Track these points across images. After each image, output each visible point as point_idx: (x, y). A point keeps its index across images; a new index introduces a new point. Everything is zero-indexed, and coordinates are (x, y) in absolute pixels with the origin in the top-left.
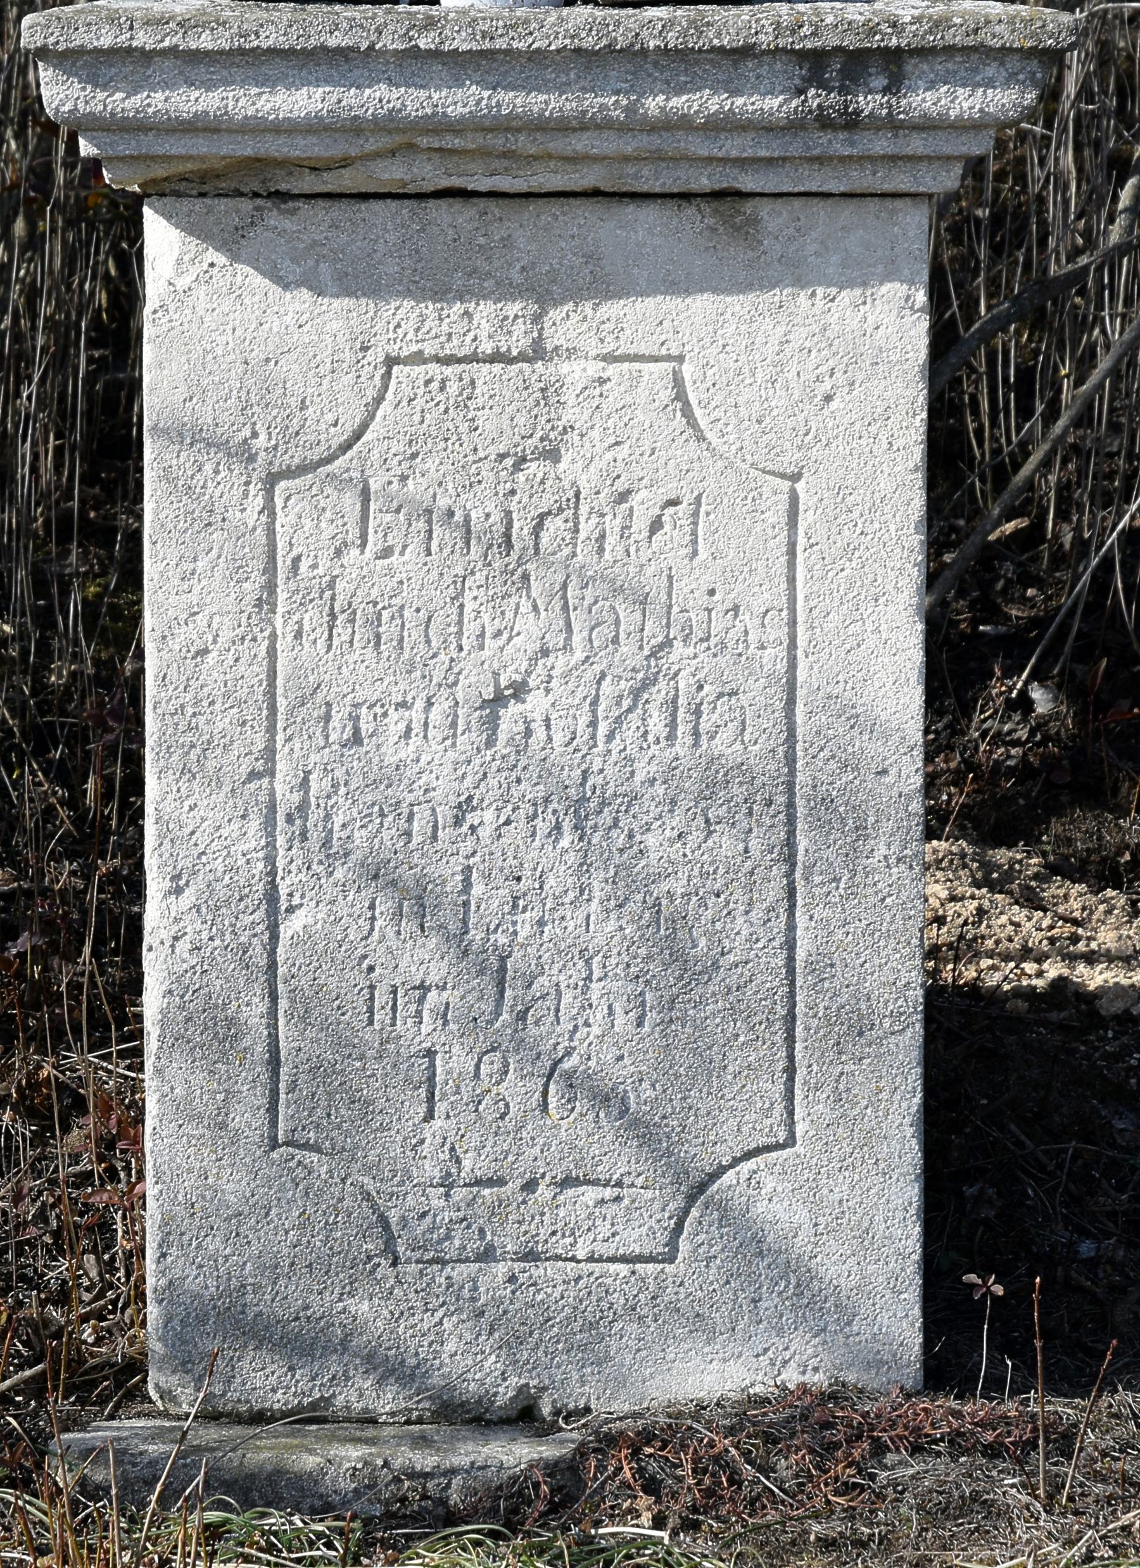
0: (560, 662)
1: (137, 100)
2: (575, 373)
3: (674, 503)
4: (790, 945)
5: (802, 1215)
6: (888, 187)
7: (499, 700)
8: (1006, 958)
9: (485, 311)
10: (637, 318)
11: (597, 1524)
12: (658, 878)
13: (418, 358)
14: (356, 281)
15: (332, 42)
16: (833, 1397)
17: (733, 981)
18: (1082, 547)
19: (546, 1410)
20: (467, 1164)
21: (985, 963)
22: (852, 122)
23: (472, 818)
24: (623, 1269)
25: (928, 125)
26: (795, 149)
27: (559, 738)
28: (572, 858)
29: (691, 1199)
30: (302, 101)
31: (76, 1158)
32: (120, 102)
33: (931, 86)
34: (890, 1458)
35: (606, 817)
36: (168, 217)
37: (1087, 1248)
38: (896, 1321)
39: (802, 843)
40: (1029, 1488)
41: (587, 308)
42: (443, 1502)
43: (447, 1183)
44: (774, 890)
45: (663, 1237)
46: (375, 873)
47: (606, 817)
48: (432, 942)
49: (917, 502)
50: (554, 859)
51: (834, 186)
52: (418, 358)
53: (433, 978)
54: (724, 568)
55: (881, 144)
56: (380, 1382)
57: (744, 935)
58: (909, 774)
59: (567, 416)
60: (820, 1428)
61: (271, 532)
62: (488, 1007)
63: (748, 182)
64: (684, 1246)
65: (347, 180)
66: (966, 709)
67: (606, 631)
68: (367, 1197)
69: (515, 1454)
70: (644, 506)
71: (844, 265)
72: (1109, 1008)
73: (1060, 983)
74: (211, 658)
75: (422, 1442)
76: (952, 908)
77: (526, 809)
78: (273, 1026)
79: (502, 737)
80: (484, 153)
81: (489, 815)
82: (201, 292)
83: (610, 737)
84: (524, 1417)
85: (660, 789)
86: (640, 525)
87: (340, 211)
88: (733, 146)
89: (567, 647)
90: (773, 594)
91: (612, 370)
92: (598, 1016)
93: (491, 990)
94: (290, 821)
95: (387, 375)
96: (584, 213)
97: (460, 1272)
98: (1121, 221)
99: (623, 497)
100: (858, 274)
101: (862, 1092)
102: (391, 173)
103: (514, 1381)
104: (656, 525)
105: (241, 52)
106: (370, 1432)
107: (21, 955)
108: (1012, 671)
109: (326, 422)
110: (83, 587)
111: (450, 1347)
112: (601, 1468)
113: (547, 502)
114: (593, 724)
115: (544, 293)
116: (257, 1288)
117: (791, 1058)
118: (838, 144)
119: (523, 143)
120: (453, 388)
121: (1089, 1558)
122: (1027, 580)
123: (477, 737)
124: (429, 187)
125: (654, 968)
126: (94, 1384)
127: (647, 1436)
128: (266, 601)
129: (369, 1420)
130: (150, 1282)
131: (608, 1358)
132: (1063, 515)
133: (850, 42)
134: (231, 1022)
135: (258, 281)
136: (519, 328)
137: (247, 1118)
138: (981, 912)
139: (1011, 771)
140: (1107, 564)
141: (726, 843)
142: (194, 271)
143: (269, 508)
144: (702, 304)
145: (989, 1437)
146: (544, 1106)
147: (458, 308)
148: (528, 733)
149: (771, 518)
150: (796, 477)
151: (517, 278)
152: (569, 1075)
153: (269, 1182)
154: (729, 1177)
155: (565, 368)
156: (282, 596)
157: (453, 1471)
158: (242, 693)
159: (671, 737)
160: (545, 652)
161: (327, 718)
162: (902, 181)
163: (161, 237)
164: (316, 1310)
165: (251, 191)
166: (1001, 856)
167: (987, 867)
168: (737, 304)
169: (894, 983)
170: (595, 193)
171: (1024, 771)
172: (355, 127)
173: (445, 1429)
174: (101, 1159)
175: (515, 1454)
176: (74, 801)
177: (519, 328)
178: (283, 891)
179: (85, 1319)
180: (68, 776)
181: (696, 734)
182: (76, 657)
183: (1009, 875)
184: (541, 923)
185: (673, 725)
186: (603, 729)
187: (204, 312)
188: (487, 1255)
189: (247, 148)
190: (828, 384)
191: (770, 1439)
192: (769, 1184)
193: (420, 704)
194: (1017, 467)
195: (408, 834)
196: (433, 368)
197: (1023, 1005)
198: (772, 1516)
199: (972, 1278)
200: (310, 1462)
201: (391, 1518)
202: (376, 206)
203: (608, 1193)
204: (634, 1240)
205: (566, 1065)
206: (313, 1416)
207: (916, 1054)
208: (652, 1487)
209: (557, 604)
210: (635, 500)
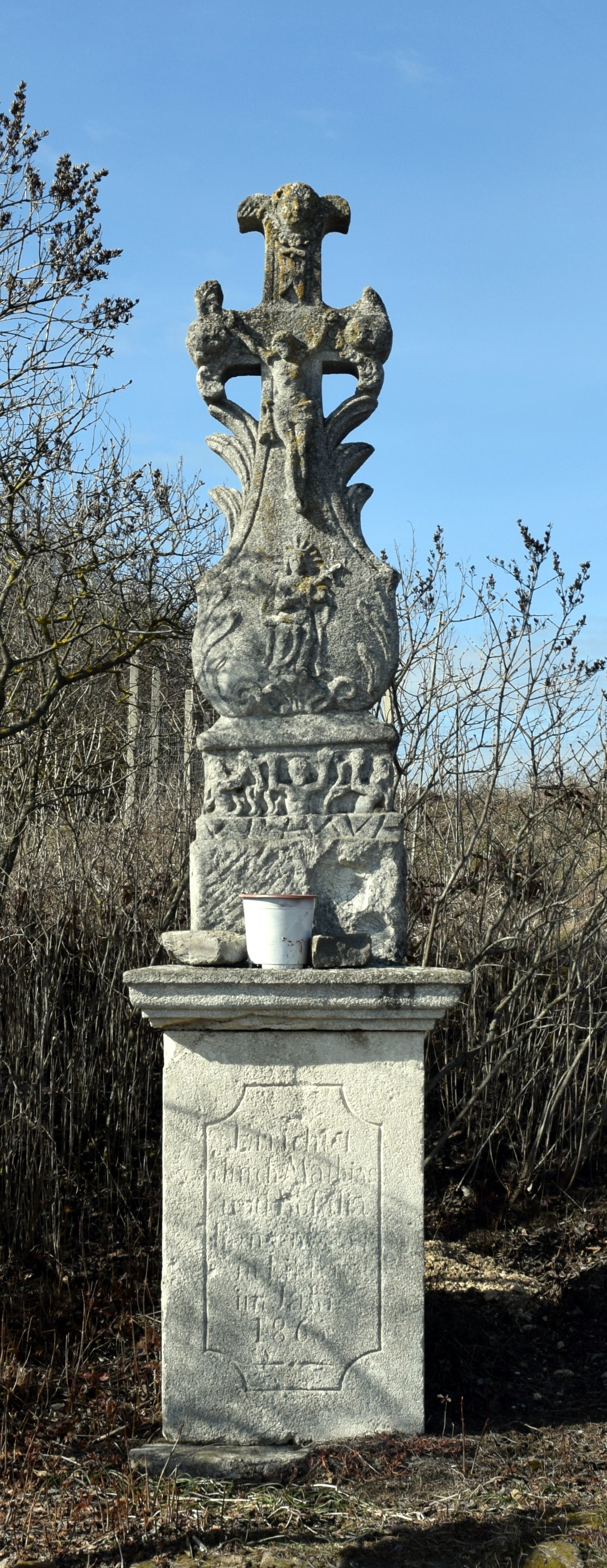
0: (302, 1187)
1: (161, 999)
2: (307, 1089)
3: (340, 1133)
4: (379, 1282)
5: (383, 1374)
6: (410, 1028)
7: (281, 1199)
8: (454, 1280)
9: (277, 1069)
10: (327, 1071)
11: (313, 1482)
12: (335, 1259)
13: (254, 1085)
14: (235, 1059)
15: (226, 980)
16: (394, 1436)
17: (360, 1294)
18: (479, 1141)
19: (297, 1441)
20: (270, 1357)
21: (447, 1282)
22: (398, 1007)
23: (272, 1239)
24: (323, 1393)
25: (424, 1008)
26: (379, 1016)
27: (301, 1212)
28: (306, 1253)
29: (346, 1369)
30: (216, 1000)
31: (141, 1351)
32: (155, 1000)
33: (424, 995)
34: (413, 1458)
35: (317, 1239)
36: (172, 1037)
37: (480, 1381)
38: (416, 1410)
39: (383, 1248)
40: (460, 1469)
41: (311, 1068)
42: (261, 1473)
43: (264, 1363)
44: (374, 1264)
45: (336, 1382)
46: (239, 1258)
47: (317, 1239)
48: (259, 1281)
49: (421, 1133)
50: (300, 1253)
51: (283, 1027)
52: (254, 1085)
53: (259, 1293)
54: (357, 1154)
55: (408, 1015)
56: (241, 1432)
57: (365, 1278)
58: (418, 1224)
59: (304, 1104)
60: (388, 1447)
61: (205, 1143)
62: (277, 1303)
64: (344, 1385)
66: (441, 1195)
67: (317, 1176)
68: (237, 1368)
69: (286, 1457)
70: (329, 1134)
71: (396, 1054)
72: (488, 1298)
73: (472, 1289)
74: (185, 1185)
75: (254, 1453)
76: (436, 1264)
77: (290, 1236)
78: (205, 1309)
79: (282, 1212)
80: (277, 1017)
81: (278, 1238)
82: (182, 1062)
83: (319, 1212)
84: (289, 1443)
85: (335, 1229)
86: (328, 1141)
87: (229, 1036)
88: (359, 1015)
89: (304, 1181)
90: (371, 1164)
91: (320, 1089)
92: (315, 1306)
93: (278, 1298)
94: (211, 1241)
95: (244, 1091)
96: (310, 1036)
97: (268, 1394)
98: (491, 1033)
99: (323, 1131)
100: (400, 1057)
101: (403, 1332)
102: (246, 1023)
103: (286, 1431)
104: (334, 1141)
105: (196, 984)
106: (237, 1449)
107: (124, 1281)
108: (457, 1182)
109: (222, 1108)
110: (149, 1153)
111: (265, 1419)
112: (315, 1462)
113: (298, 1132)
114: (313, 1207)
115: (296, 1062)
116: (199, 1399)
117: (380, 1320)
118: (393, 1014)
119: (289, 1014)
120: (266, 1095)
121: (479, 1494)
122: (461, 1151)
123: (274, 1212)
124: (258, 1028)
125: (334, 1290)
126: (144, 1431)
127: (331, 1451)
128: (203, 1166)
129: (237, 1444)
130: (163, 1396)
131: (318, 1423)
132: (472, 1130)
133: (397, 981)
134: (191, 1308)
135: (201, 1059)
136: (288, 1075)
137: (196, 1341)
138: (445, 1265)
139: (456, 1216)
140: (487, 1146)
141: (358, 1248)
142: (180, 1055)
143: (204, 1134)
144: (349, 1067)
145: (446, 1451)
146: (296, 1337)
147: (268, 1068)
148: (291, 1210)
149: (372, 1138)
150: (380, 1125)
151: (287, 1058)
152: (305, 1326)
153: (203, 1363)
154: (359, 1361)
155: (303, 1088)
156: (209, 1164)
157: (265, 1463)
158: (195, 1197)
159: (339, 1212)
160: (297, 1183)
161: (224, 1205)
162: (414, 1026)
163: (169, 1044)
164: (219, 1406)
165: (199, 1029)
166: (453, 1245)
167: (448, 1249)
168: (362, 1067)
169: (415, 1293)
170: (313, 1030)
171: (460, 1216)
172: (233, 1008)
173: (263, 1448)
174: (149, 1351)
175: (286, 1457)
176: (144, 1226)
177: (288, 1075)
178: (208, 1264)
179: (142, 1407)
180: (142, 1217)
181: (347, 1211)
182: (146, 1176)
183: (455, 1252)
184: (295, 1275)
185: (339, 1208)
186: (316, 1209)
187: (183, 1070)
188: (277, 1388)
189: (198, 1015)
190: (391, 1094)
191: (372, 1452)
192: (372, 1363)
193: (255, 1201)
194: (458, 1113)
195: (251, 1245)
196: (259, 1088)
197: (459, 1297)
198: (373, 1479)
199: (441, 1396)
200: (216, 1460)
201: (244, 1479)
202: (241, 1034)
203: (318, 1367)
204: (327, 1382)
205: (304, 1323)
206: (217, 1443)
207: (422, 1319)
208: (332, 1469)
209: (301, 1167)
210: (327, 1132)
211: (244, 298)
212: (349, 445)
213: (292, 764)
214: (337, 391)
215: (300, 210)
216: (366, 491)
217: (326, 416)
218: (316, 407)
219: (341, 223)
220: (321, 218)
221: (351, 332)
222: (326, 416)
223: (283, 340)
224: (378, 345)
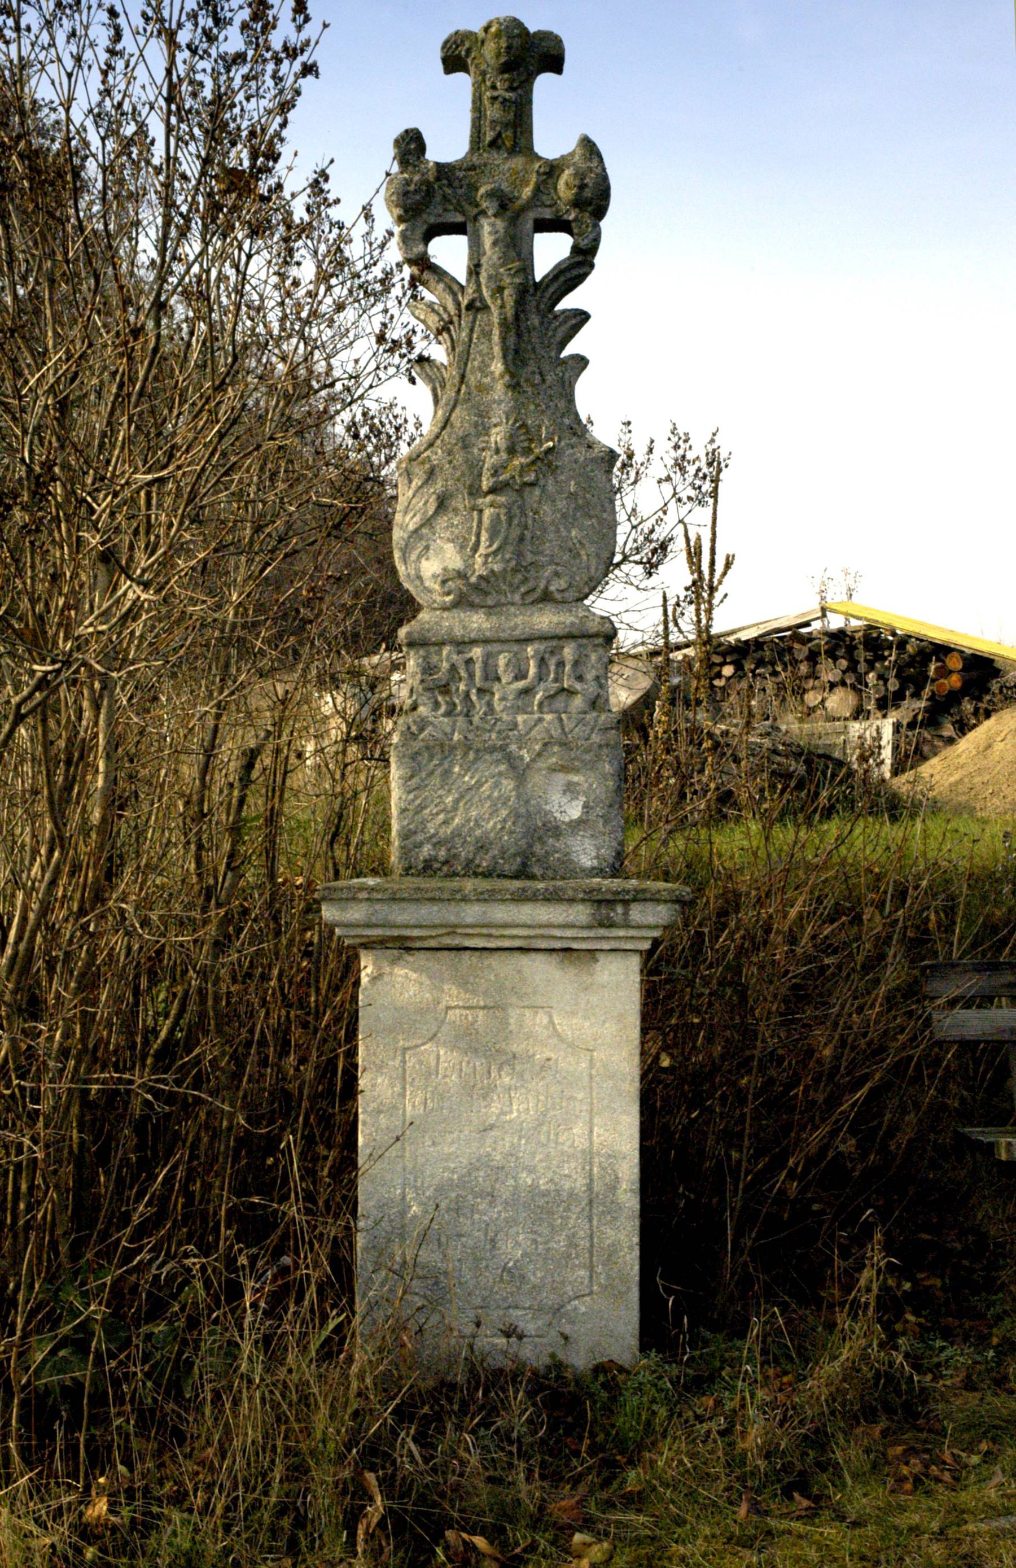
51: (490, 945)
63: (575, 946)
65: (433, 943)
87: (428, 954)
88: (569, 933)
96: (517, 955)
143: (404, 1062)
170: (520, 949)
211: (448, 144)
212: (564, 311)
213: (502, 661)
214: (550, 250)
215: (509, 48)
216: (581, 362)
217: (538, 279)
218: (527, 266)
219: (555, 63)
220: (530, 55)
221: (564, 187)
222: (538, 279)
223: (491, 195)
224: (594, 200)
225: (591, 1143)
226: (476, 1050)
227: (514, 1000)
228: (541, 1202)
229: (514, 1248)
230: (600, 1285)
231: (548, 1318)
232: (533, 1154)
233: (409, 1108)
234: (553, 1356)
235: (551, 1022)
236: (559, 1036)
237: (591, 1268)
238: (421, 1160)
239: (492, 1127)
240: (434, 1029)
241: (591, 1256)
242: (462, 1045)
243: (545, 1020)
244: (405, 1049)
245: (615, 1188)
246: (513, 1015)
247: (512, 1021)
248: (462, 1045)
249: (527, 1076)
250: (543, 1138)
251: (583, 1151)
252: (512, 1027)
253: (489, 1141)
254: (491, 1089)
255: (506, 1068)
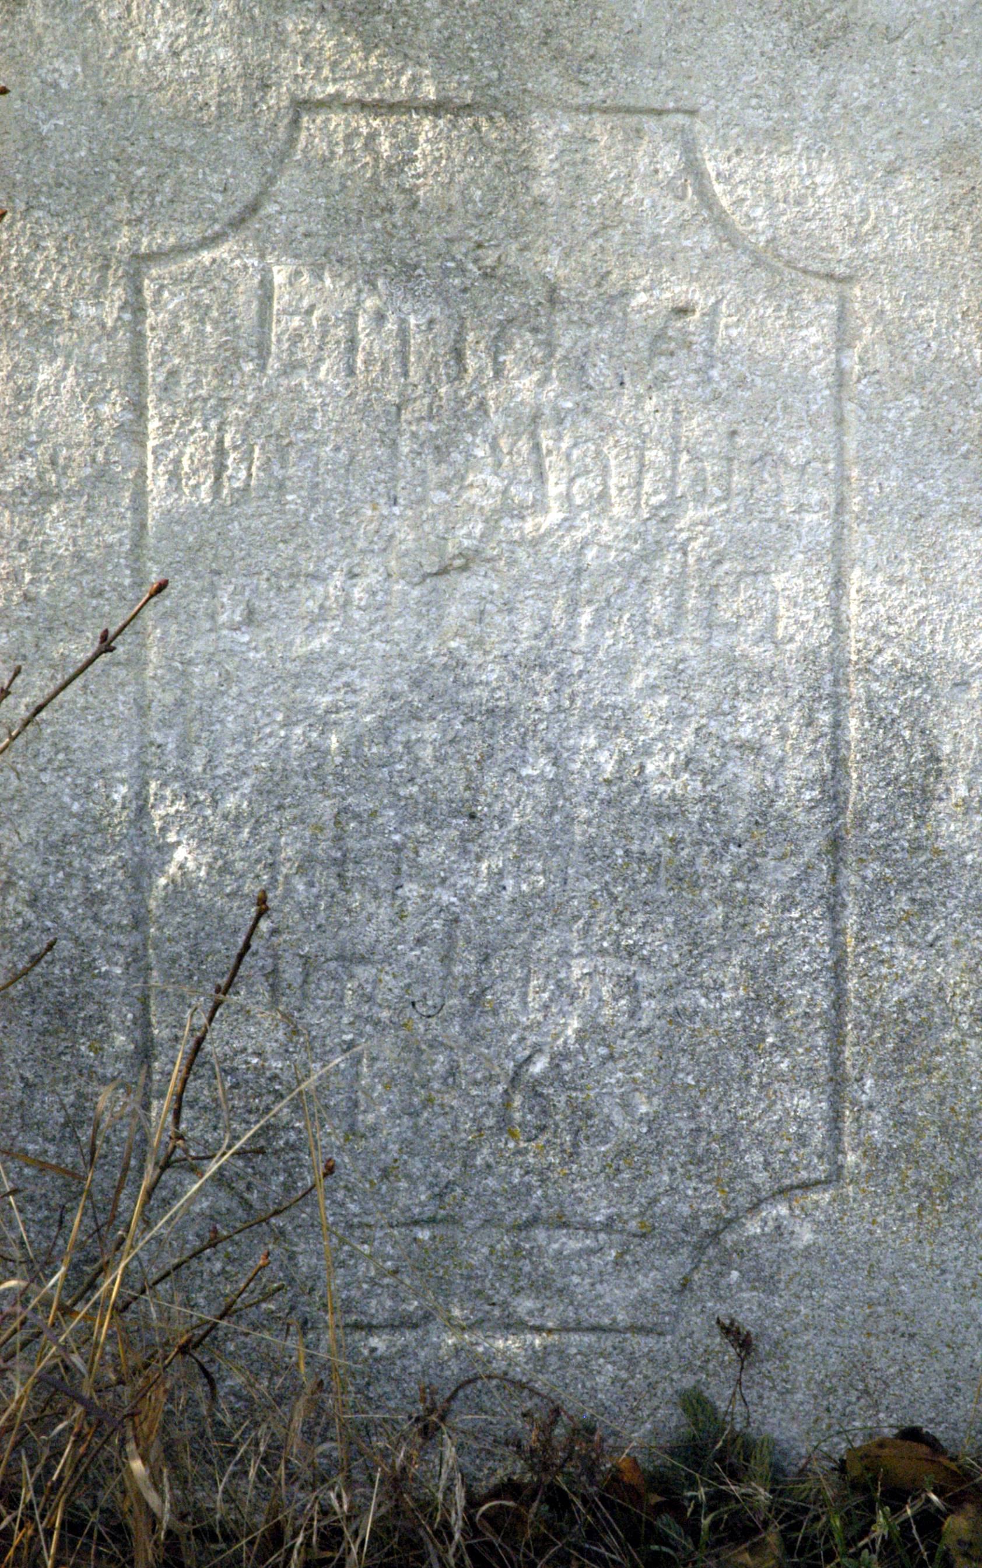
143: (136, 307)
225: (839, 629)
226: (408, 271)
227: (551, 80)
228: (655, 841)
229: (563, 1004)
230: (869, 1151)
231: (676, 1265)
232: (623, 666)
233: (157, 483)
234: (695, 1404)
235: (693, 168)
236: (720, 221)
237: (838, 1083)
238: (205, 678)
239: (469, 561)
240: (249, 186)
241: (837, 1038)
242: (358, 246)
243: (670, 164)
244: (140, 261)
245: (926, 796)
246: (549, 135)
247: (545, 160)
248: (358, 246)
249: (600, 370)
250: (658, 605)
251: (809, 656)
252: (543, 186)
253: (456, 612)
254: (468, 415)
255: (523, 340)
